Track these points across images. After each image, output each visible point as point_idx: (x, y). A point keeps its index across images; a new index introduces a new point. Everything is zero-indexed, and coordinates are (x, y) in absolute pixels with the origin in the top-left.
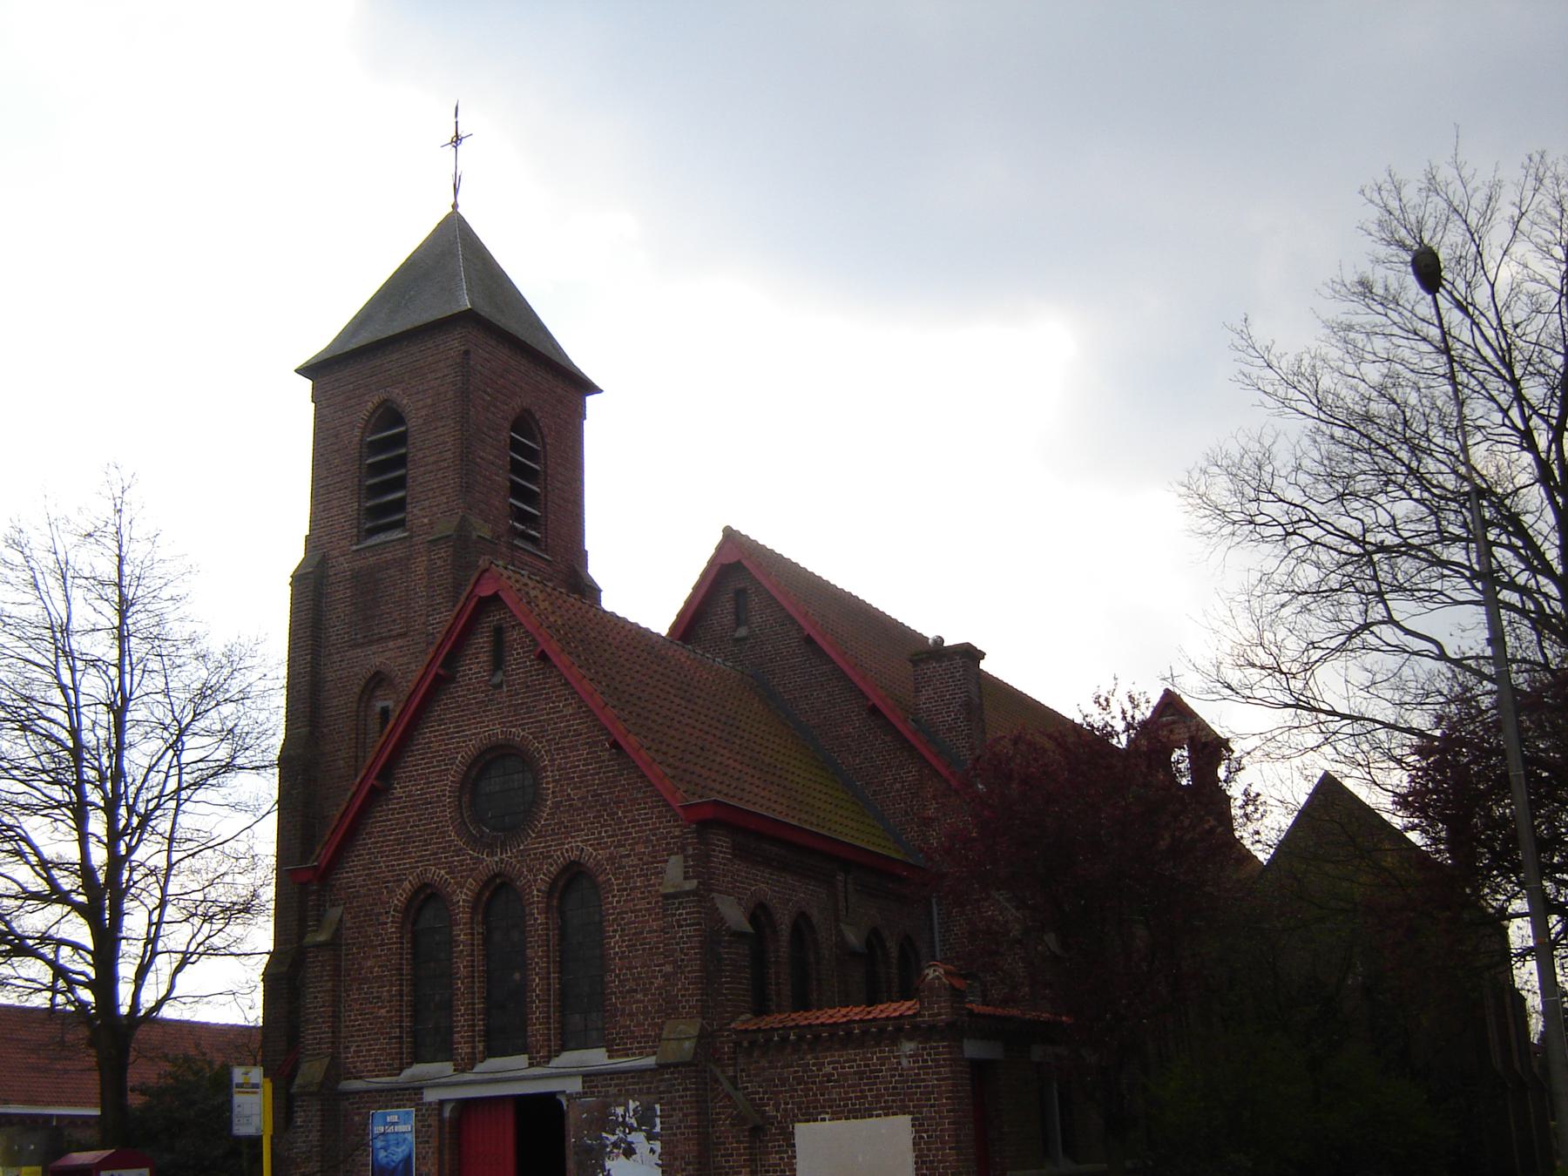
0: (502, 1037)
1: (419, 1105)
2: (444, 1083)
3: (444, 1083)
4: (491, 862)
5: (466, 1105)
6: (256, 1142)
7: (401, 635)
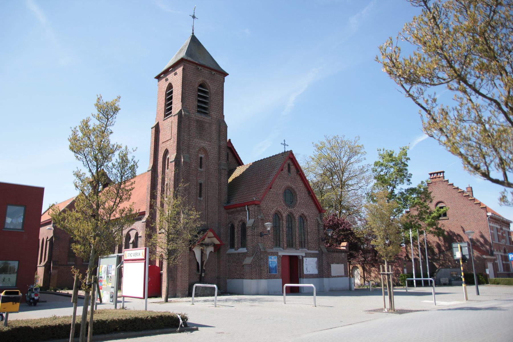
1: (278, 256)
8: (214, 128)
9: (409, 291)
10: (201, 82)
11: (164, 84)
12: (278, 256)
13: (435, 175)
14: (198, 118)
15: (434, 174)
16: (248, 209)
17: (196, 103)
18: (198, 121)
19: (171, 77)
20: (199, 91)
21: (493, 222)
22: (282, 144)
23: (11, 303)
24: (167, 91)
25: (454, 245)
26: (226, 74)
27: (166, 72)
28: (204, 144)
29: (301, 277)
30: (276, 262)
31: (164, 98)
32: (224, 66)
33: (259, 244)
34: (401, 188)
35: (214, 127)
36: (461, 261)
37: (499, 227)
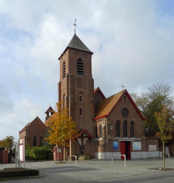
0: (125, 135)
1: (118, 141)
2: (121, 139)
3: (121, 139)
4: (125, 119)
5: (121, 141)
6: (165, 146)
7: (84, 88)
17: (76, 69)
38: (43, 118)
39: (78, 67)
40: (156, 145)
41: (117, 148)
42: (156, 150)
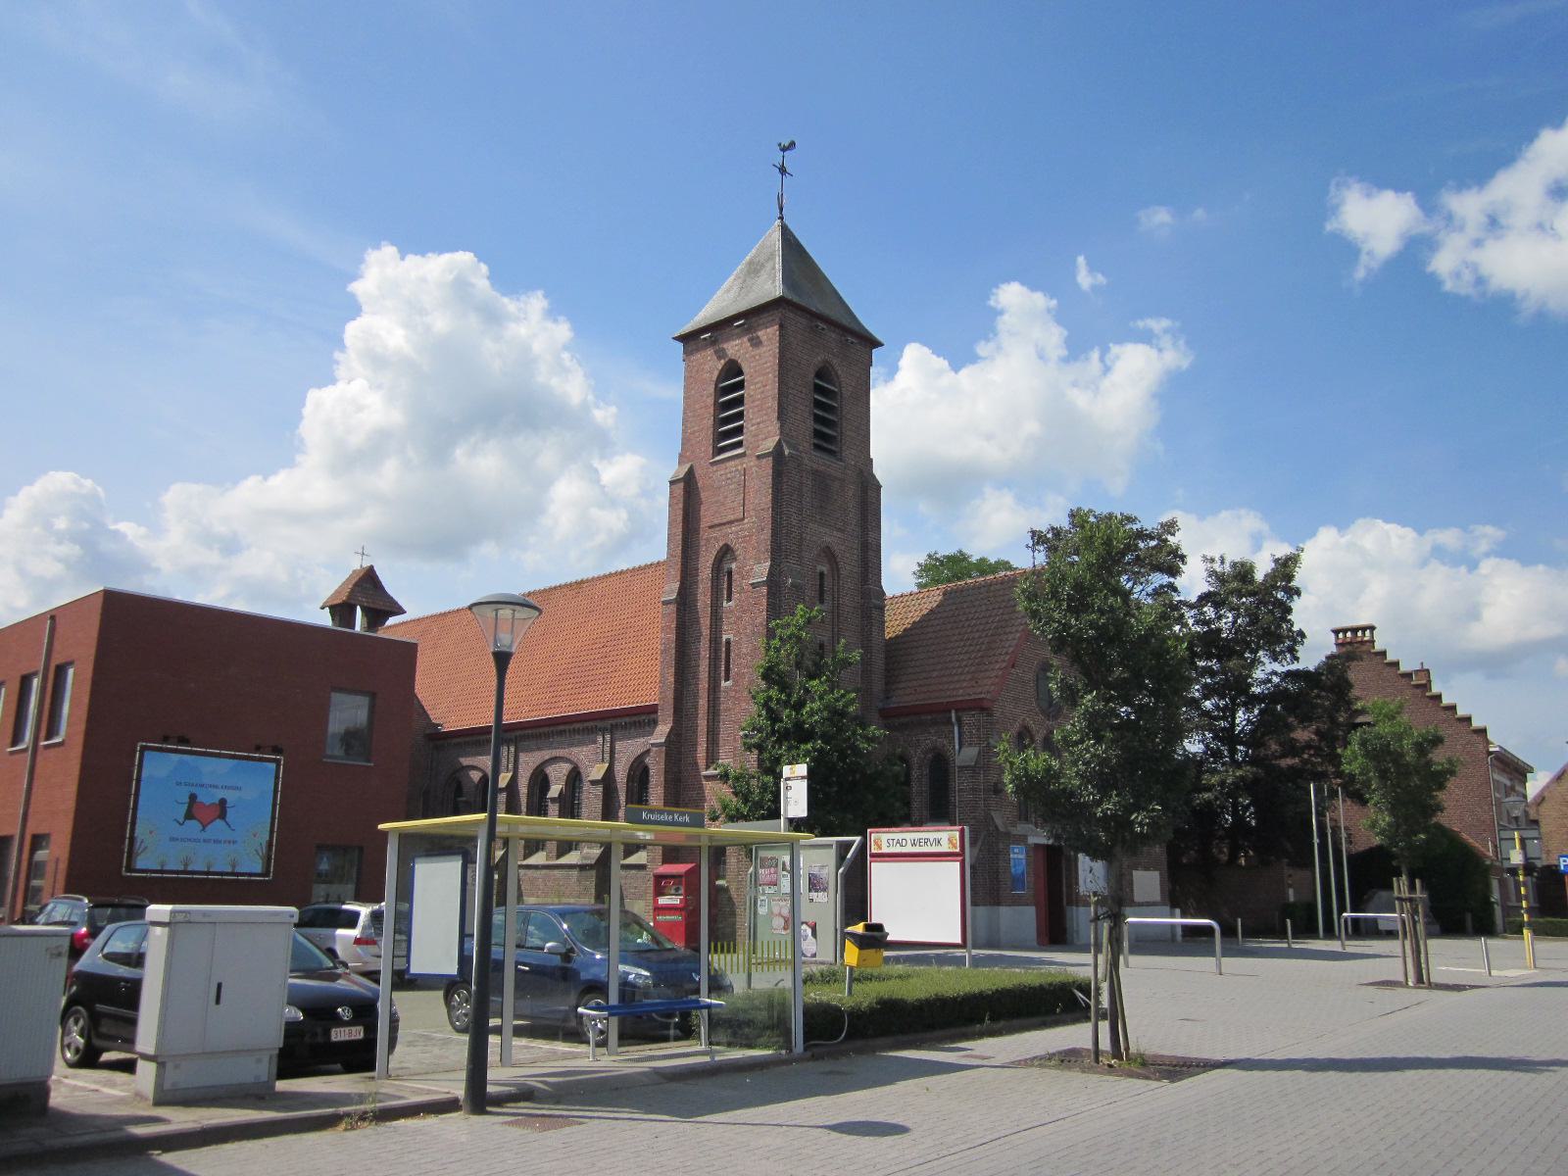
1: (1026, 844)
5: (1035, 844)
8: (850, 493)
9: (1349, 950)
10: (821, 365)
11: (710, 364)
12: (1026, 844)
13: (1349, 634)
14: (815, 466)
15: (1345, 631)
16: (959, 720)
17: (811, 424)
18: (815, 473)
19: (735, 347)
20: (818, 389)
21: (1498, 768)
22: (1027, 546)
23: (874, 950)
24: (720, 379)
25: (787, 770)
26: (877, 344)
27: (719, 329)
28: (831, 538)
29: (1070, 903)
30: (1024, 862)
31: (710, 401)
32: (871, 322)
33: (993, 813)
34: (1267, 670)
35: (851, 491)
36: (1520, 872)
37: (1508, 783)
38: (337, 355)
39: (817, 381)
40: (1157, 873)
41: (1017, 881)
42: (1158, 898)
